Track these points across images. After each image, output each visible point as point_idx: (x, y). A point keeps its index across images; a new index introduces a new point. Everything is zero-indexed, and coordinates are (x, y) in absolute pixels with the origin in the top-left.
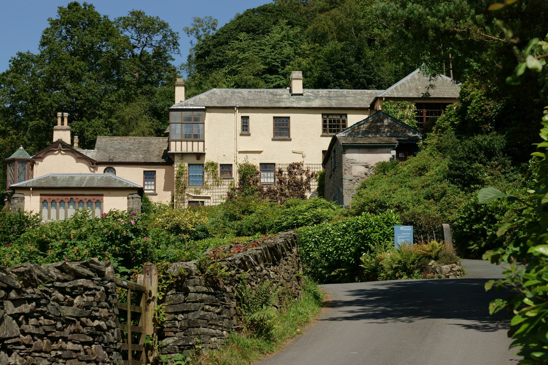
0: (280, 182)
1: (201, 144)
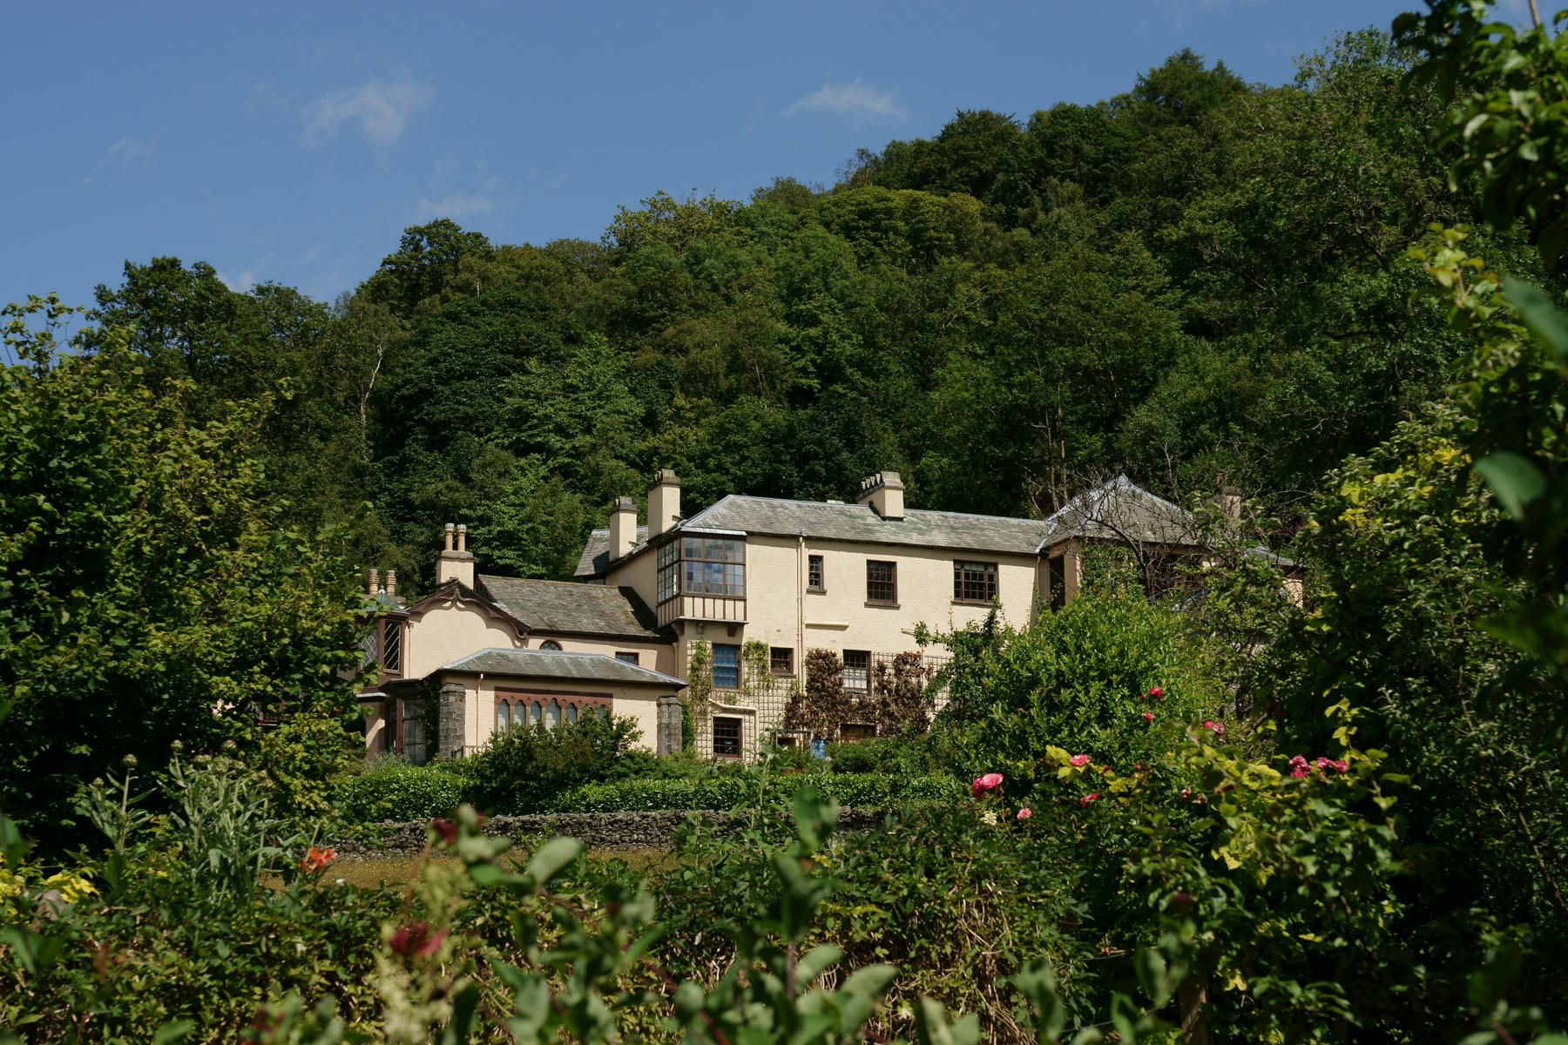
0: (883, 687)
1: (740, 604)
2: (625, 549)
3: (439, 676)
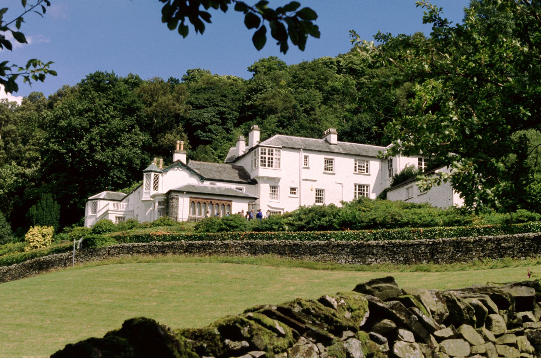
2: (241, 153)
3: (170, 192)
